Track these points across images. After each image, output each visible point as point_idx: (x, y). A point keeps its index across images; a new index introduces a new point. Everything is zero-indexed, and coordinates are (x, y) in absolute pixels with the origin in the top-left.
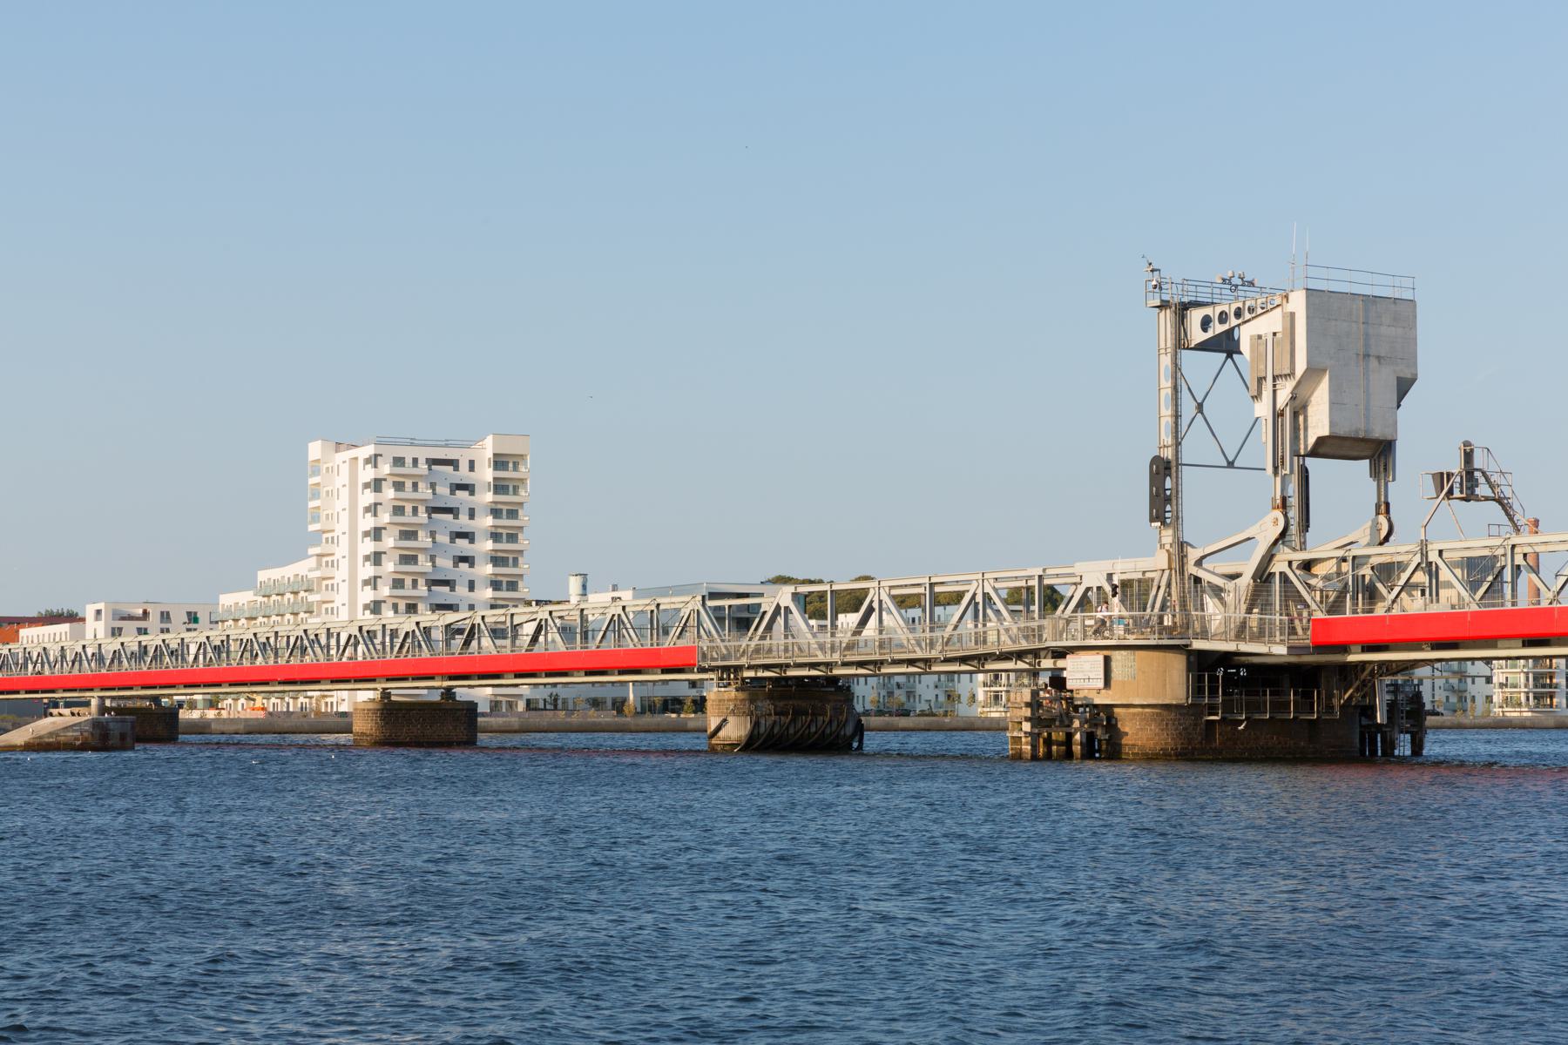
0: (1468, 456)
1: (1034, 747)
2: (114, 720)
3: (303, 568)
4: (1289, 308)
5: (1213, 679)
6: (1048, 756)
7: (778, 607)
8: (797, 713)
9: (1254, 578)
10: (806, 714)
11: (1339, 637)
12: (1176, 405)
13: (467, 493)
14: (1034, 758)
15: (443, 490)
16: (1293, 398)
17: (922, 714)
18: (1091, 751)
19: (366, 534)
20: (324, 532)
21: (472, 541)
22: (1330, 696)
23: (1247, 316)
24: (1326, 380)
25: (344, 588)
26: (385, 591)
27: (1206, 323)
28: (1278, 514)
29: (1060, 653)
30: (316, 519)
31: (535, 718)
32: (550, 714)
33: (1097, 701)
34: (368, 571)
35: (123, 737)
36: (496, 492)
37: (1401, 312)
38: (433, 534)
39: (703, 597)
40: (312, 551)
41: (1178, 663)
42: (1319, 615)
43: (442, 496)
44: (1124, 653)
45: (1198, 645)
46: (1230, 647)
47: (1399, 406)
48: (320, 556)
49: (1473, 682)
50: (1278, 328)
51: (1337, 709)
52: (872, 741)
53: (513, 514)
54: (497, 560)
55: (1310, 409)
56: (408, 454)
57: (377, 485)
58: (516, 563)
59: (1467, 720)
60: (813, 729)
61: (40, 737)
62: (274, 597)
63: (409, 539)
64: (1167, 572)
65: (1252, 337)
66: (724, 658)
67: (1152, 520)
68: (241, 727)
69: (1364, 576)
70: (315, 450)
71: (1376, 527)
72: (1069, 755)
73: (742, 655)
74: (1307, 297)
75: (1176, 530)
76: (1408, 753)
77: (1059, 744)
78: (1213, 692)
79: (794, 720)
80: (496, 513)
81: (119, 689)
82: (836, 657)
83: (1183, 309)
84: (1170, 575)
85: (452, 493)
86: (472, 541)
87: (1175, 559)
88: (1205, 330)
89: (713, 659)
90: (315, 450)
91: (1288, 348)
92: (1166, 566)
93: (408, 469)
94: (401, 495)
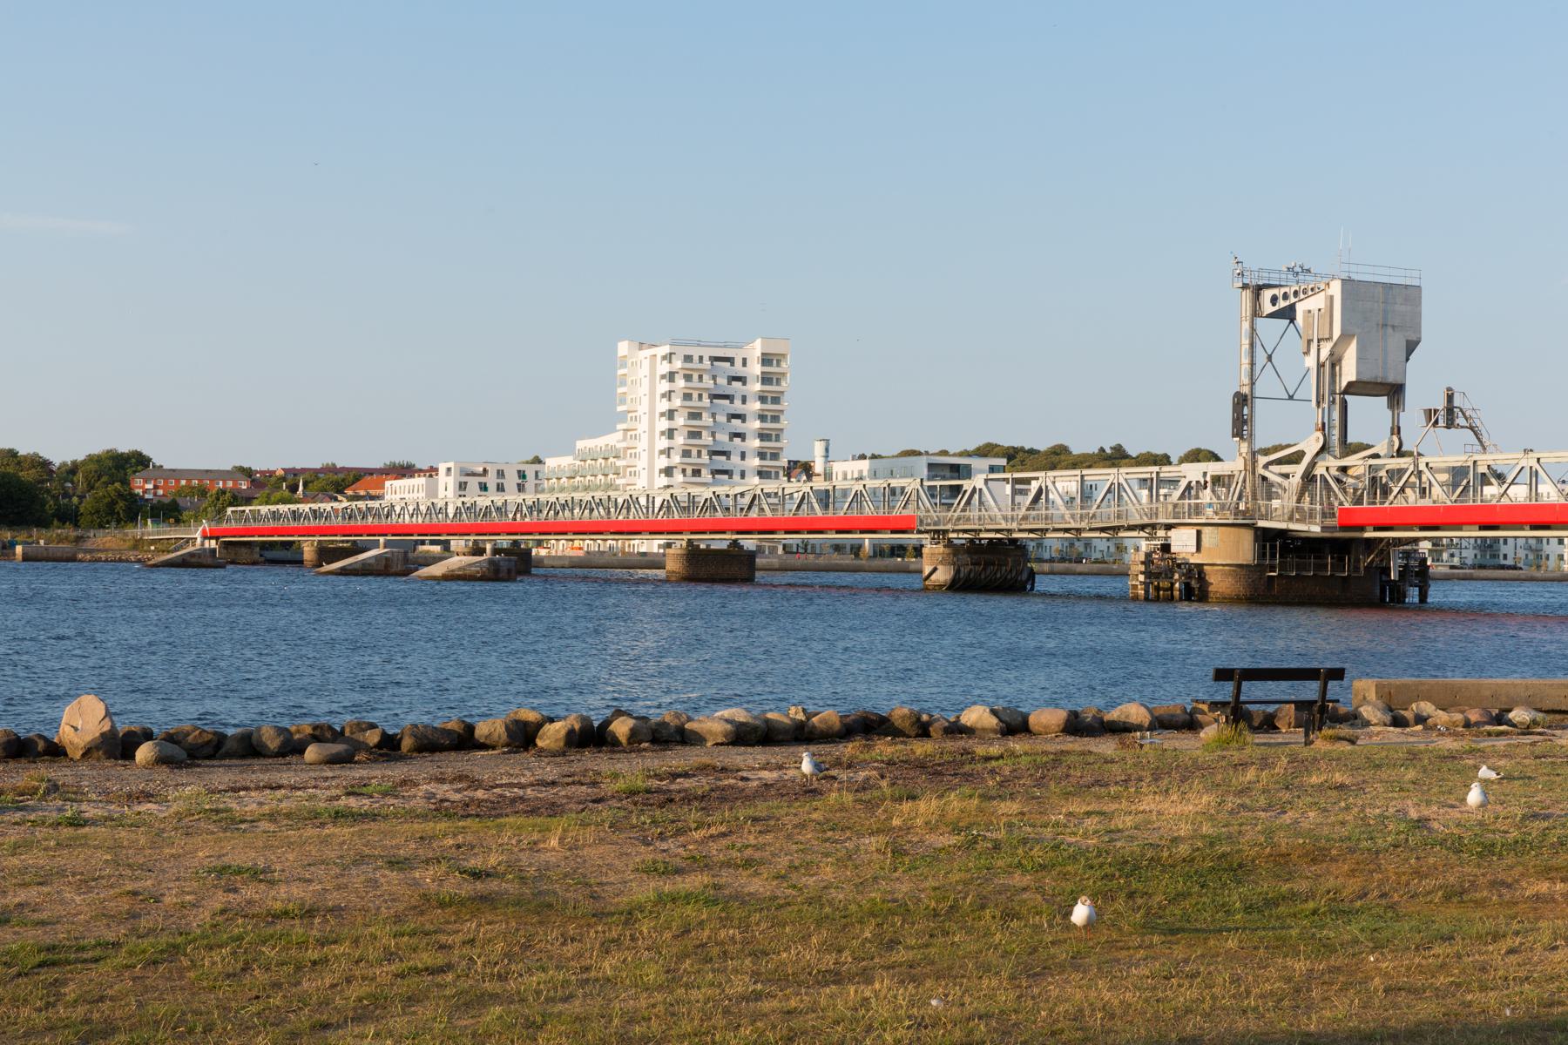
0: (1450, 398)
1: (1147, 591)
2: (503, 560)
3: (613, 440)
4: (1330, 292)
5: (1273, 547)
6: (1157, 599)
7: (974, 489)
8: (987, 564)
9: (1302, 478)
10: (994, 564)
11: (1358, 520)
12: (1252, 357)
13: (740, 383)
14: (1147, 599)
15: (722, 381)
16: (1332, 354)
17: (1096, 561)
18: (1189, 594)
19: (662, 414)
20: (629, 412)
21: (744, 421)
22: (1358, 561)
23: (1302, 296)
24: (1355, 341)
25: (645, 456)
26: (676, 459)
27: (1274, 300)
28: (1319, 434)
29: (1169, 527)
30: (623, 402)
31: (792, 560)
32: (802, 556)
33: (1192, 561)
34: (664, 443)
35: (509, 571)
36: (763, 383)
37: (1411, 294)
38: (713, 415)
39: (922, 480)
40: (620, 426)
41: (1247, 537)
42: (1347, 505)
43: (722, 386)
44: (1210, 528)
45: (1262, 524)
46: (1282, 526)
47: (1407, 360)
48: (626, 430)
49: (1548, 543)
50: (1322, 306)
51: (1362, 569)
52: (1042, 584)
53: (776, 400)
54: (763, 436)
55: (1343, 362)
56: (695, 352)
57: (671, 377)
58: (778, 439)
59: (1541, 574)
60: (998, 575)
61: (453, 571)
62: (589, 462)
63: (695, 419)
64: (1243, 473)
65: (1304, 312)
66: (935, 524)
67: (1234, 436)
68: (567, 563)
69: (1381, 477)
70: (623, 348)
71: (1391, 443)
72: (1171, 599)
73: (948, 522)
74: (1342, 285)
75: (1250, 443)
76: (1416, 600)
77: (1165, 590)
78: (1273, 556)
79: (984, 569)
80: (763, 399)
81: (490, 535)
82: (1014, 526)
83: (1258, 290)
84: (1245, 475)
85: (729, 383)
86: (744, 421)
87: (1249, 463)
88: (1274, 305)
89: (929, 525)
90: (623, 348)
91: (1328, 325)
92: (1242, 468)
93: (695, 365)
94: (690, 384)
